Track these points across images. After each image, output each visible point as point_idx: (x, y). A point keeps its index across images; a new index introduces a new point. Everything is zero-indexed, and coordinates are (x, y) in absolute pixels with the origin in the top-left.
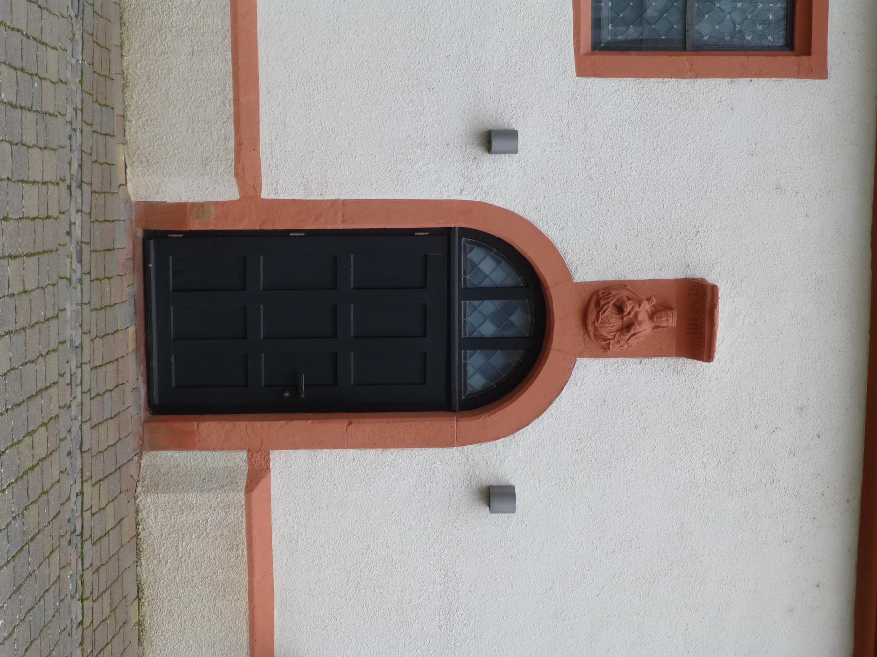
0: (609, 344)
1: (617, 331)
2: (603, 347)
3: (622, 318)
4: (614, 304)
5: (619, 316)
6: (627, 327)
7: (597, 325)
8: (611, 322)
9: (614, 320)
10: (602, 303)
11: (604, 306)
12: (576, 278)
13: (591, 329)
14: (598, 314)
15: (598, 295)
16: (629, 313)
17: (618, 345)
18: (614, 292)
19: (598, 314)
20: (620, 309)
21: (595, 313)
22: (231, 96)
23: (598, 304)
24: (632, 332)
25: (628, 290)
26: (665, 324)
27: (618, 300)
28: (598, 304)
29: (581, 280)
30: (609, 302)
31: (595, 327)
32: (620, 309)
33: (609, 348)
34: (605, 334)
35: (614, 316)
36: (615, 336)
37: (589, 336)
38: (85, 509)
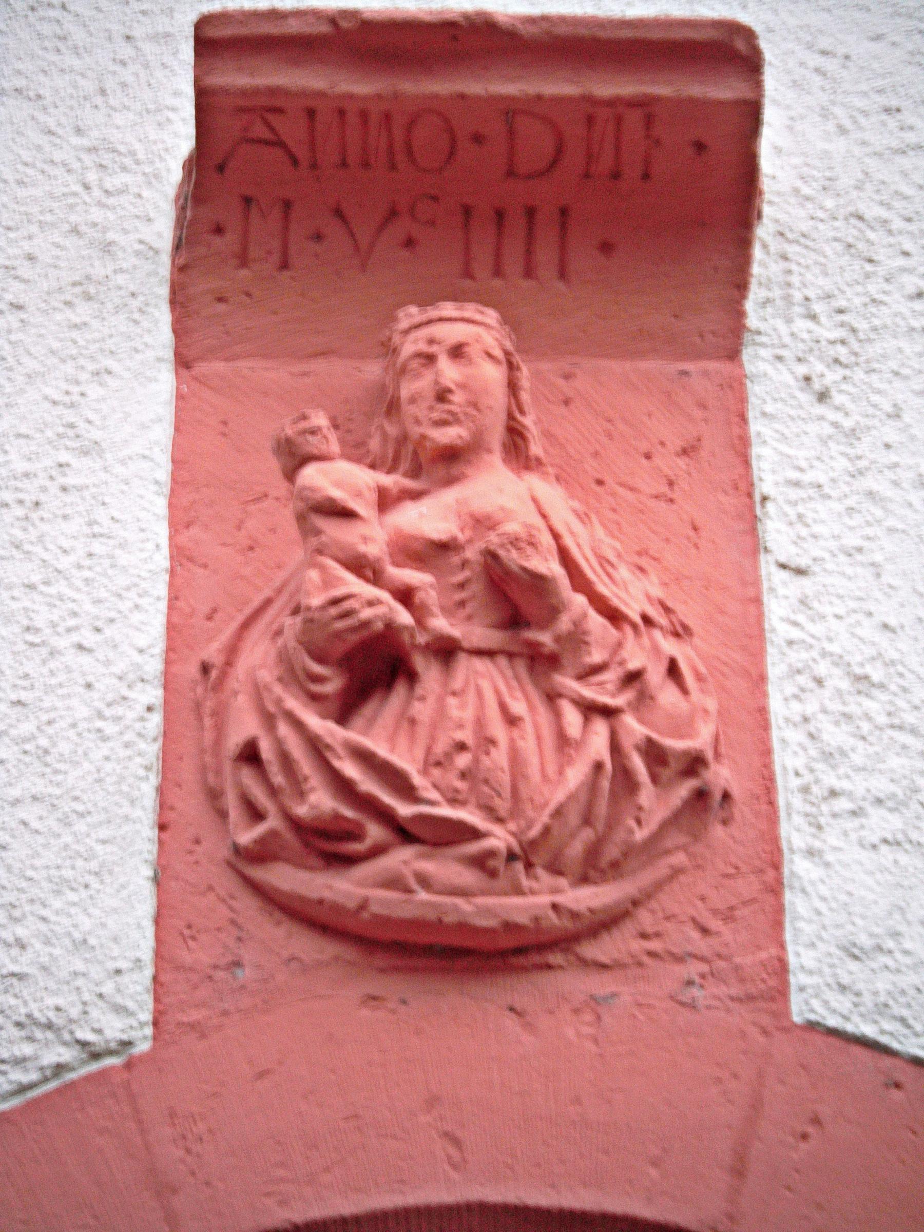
0: (654, 754)
1: (552, 697)
2: (698, 800)
3: (446, 651)
4: (343, 717)
5: (429, 673)
6: (516, 605)
7: (499, 838)
8: (468, 721)
9: (461, 711)
10: (320, 801)
11: (344, 787)
12: (114, 1028)
13: (538, 899)
14: (404, 833)
15: (261, 854)
16: (405, 596)
17: (668, 697)
18: (245, 725)
19: (404, 833)
20: (373, 667)
21: (403, 859)
22: (849, 1028)
23: (328, 844)
24: (553, 568)
25: (232, 651)
26: (493, 375)
27: (303, 684)
28: (328, 844)
29: (137, 990)
30: (317, 747)
31: (524, 855)
32: (373, 667)
33: (694, 764)
34: (576, 775)
35: (422, 711)
36: (592, 710)
37: (605, 923)
38: (266, 135)
